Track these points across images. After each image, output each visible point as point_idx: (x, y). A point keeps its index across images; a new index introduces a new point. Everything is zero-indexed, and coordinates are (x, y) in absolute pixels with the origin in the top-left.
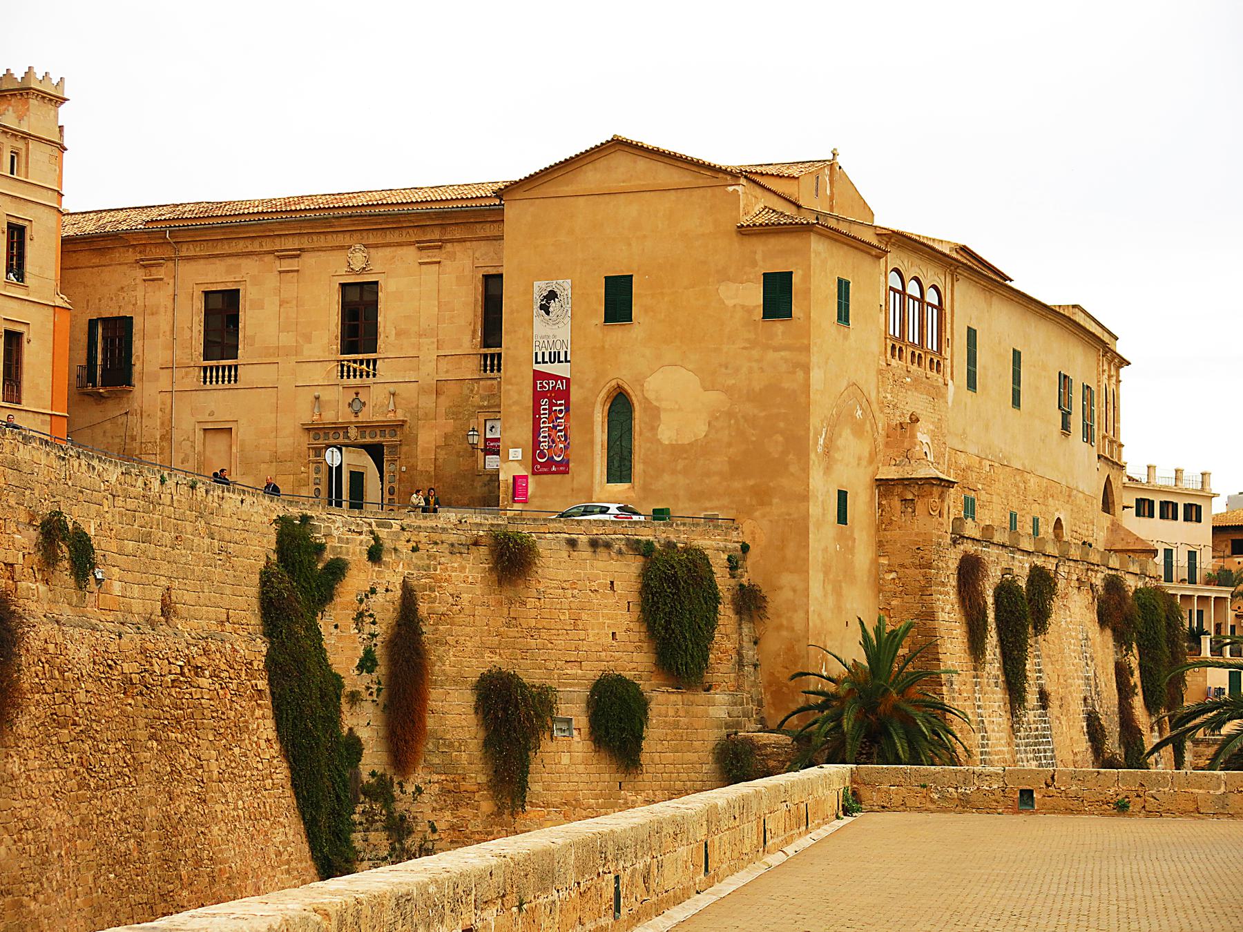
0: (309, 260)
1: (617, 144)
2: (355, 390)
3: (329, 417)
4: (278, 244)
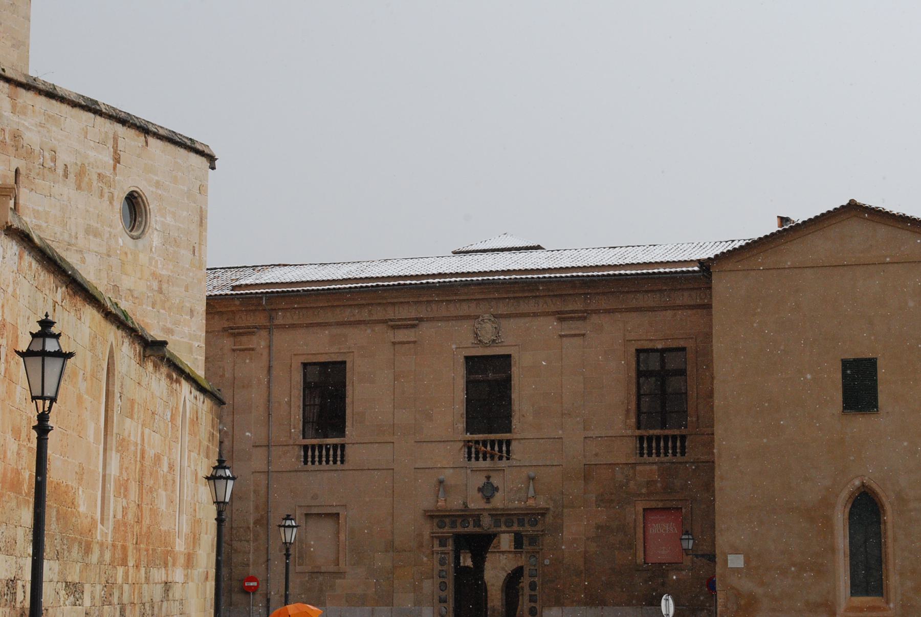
0: (427, 331)
1: (853, 209)
2: (485, 474)
3: (455, 503)
4: (390, 313)
